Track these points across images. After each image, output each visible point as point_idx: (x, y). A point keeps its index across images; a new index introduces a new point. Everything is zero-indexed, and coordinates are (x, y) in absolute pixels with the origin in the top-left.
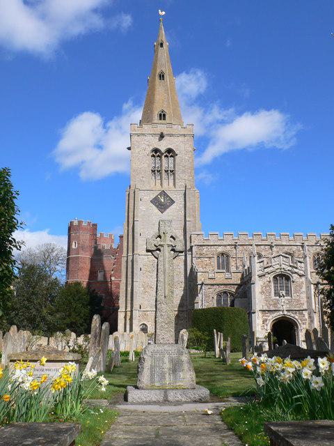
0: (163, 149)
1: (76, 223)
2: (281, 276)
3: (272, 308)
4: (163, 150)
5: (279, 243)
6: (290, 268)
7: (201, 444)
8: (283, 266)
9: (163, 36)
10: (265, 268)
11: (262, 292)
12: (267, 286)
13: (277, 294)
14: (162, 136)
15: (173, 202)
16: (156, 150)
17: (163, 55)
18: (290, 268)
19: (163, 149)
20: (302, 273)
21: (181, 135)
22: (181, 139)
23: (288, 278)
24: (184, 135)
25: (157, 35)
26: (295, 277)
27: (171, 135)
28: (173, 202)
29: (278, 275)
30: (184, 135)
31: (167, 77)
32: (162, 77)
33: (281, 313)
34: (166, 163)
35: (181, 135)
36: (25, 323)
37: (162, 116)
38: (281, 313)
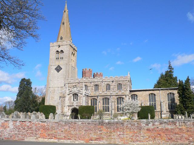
0: (59, 51)
1: (96, 74)
2: (75, 94)
3: (71, 105)
4: (59, 51)
5: (94, 81)
6: (78, 92)
7: (193, 124)
8: (76, 91)
9: (66, 9)
10: (70, 92)
11: (69, 100)
12: (70, 97)
13: (73, 100)
14: (59, 46)
15: (62, 69)
16: (58, 51)
17: (66, 15)
18: (78, 92)
19: (59, 51)
20: (82, 93)
21: (65, 45)
22: (66, 46)
23: (77, 95)
24: (67, 45)
25: (64, 8)
26: (79, 95)
27: (62, 45)
28: (62, 69)
29: (74, 94)
30: (67, 45)
31: (65, 24)
32: (63, 24)
33: (74, 106)
34: (61, 55)
35: (65, 45)
36: (24, 110)
37: (62, 38)
38: (74, 106)
